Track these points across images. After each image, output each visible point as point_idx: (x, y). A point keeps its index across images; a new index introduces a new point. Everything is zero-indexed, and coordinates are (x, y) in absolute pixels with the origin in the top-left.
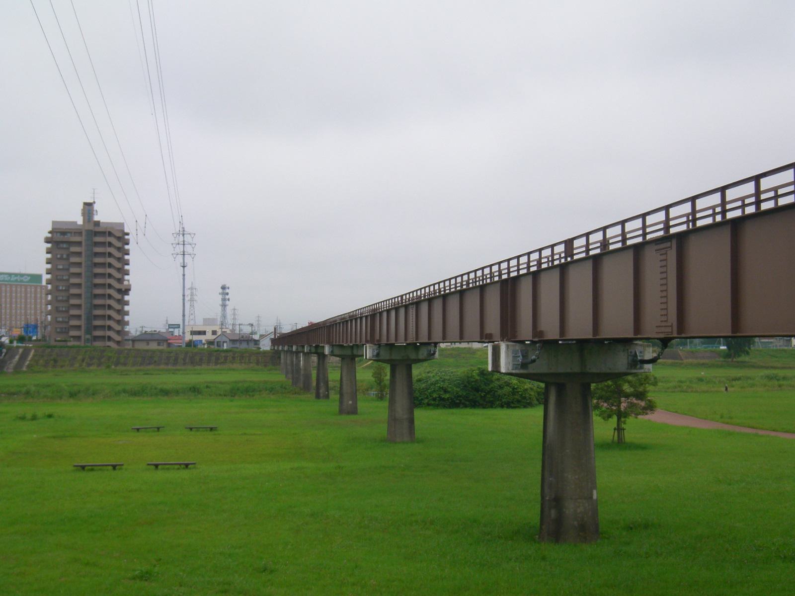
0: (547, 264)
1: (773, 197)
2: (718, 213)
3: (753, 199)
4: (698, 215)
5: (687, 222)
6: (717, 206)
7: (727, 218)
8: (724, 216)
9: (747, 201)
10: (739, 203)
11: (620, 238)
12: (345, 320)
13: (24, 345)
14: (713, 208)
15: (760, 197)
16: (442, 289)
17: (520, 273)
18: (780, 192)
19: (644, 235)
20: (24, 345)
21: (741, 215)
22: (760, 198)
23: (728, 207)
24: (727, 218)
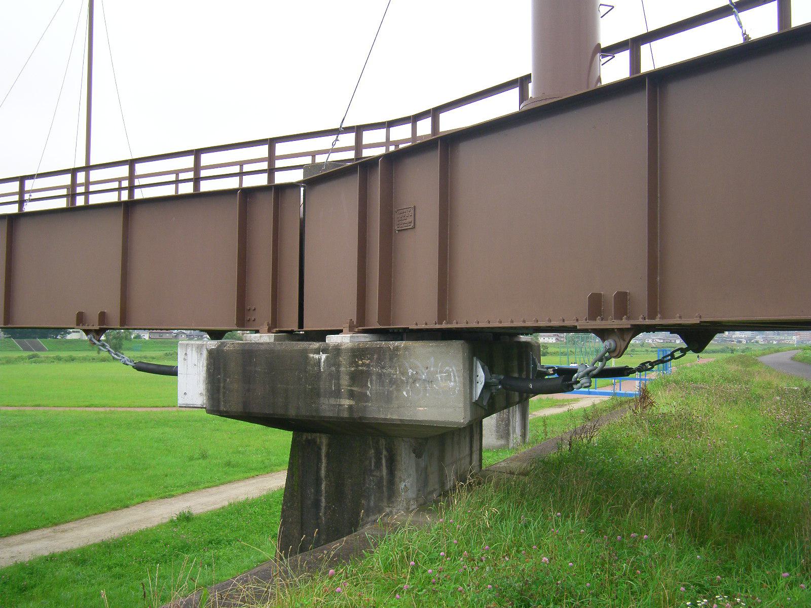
0: (310, 158)
1: (83, 193)
2: (125, 188)
3: (191, 175)
4: (92, 188)
5: (120, 189)
6: (124, 179)
7: (792, 27)
8: (131, 194)
9: (182, 176)
10: (172, 177)
11: (264, 166)
12: (511, 432)
13: (385, 483)
14: (120, 180)
15: (24, 197)
16: (80, 190)
17: (646, 67)
18: (247, 168)
19: (21, 202)
20: (385, 483)
21: (629, 76)
22: (200, 175)
23: (203, 173)
24: (792, 27)
